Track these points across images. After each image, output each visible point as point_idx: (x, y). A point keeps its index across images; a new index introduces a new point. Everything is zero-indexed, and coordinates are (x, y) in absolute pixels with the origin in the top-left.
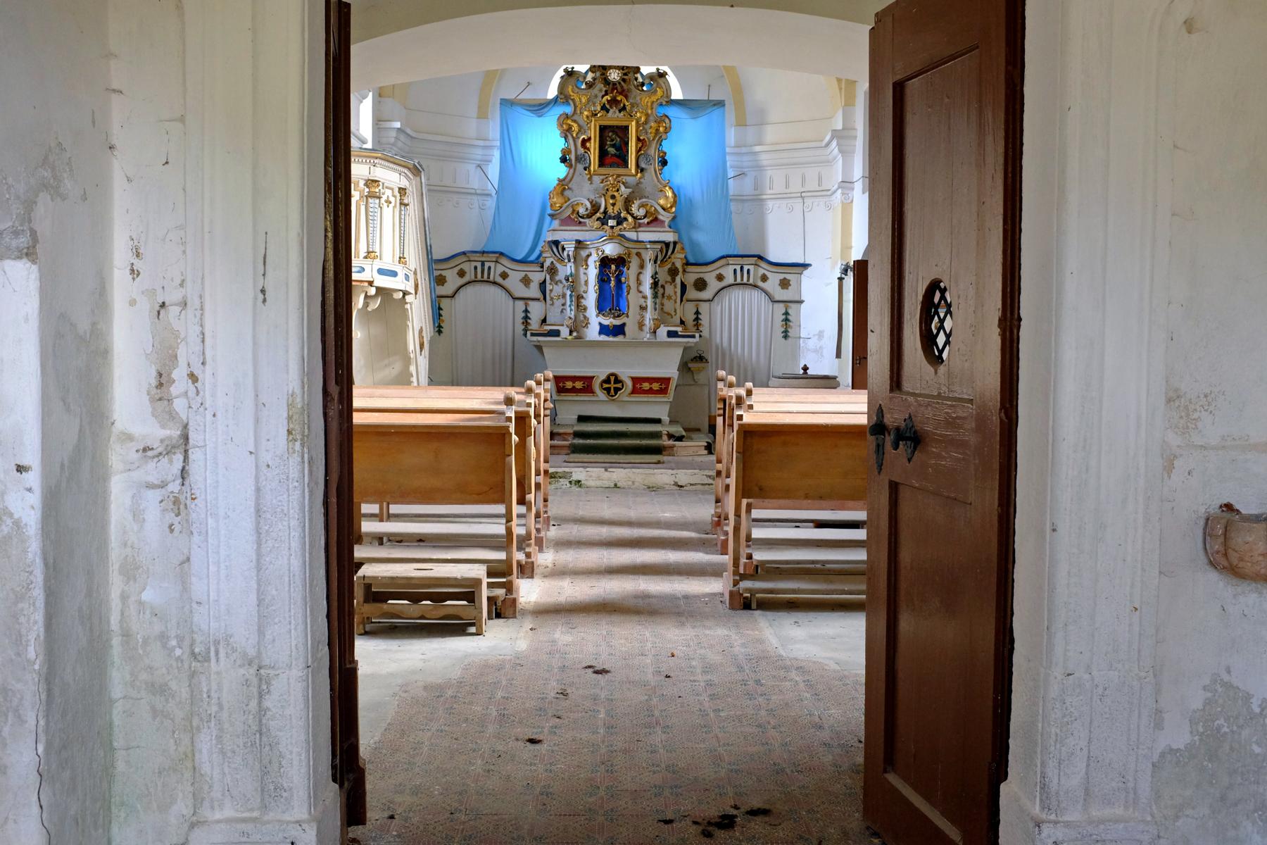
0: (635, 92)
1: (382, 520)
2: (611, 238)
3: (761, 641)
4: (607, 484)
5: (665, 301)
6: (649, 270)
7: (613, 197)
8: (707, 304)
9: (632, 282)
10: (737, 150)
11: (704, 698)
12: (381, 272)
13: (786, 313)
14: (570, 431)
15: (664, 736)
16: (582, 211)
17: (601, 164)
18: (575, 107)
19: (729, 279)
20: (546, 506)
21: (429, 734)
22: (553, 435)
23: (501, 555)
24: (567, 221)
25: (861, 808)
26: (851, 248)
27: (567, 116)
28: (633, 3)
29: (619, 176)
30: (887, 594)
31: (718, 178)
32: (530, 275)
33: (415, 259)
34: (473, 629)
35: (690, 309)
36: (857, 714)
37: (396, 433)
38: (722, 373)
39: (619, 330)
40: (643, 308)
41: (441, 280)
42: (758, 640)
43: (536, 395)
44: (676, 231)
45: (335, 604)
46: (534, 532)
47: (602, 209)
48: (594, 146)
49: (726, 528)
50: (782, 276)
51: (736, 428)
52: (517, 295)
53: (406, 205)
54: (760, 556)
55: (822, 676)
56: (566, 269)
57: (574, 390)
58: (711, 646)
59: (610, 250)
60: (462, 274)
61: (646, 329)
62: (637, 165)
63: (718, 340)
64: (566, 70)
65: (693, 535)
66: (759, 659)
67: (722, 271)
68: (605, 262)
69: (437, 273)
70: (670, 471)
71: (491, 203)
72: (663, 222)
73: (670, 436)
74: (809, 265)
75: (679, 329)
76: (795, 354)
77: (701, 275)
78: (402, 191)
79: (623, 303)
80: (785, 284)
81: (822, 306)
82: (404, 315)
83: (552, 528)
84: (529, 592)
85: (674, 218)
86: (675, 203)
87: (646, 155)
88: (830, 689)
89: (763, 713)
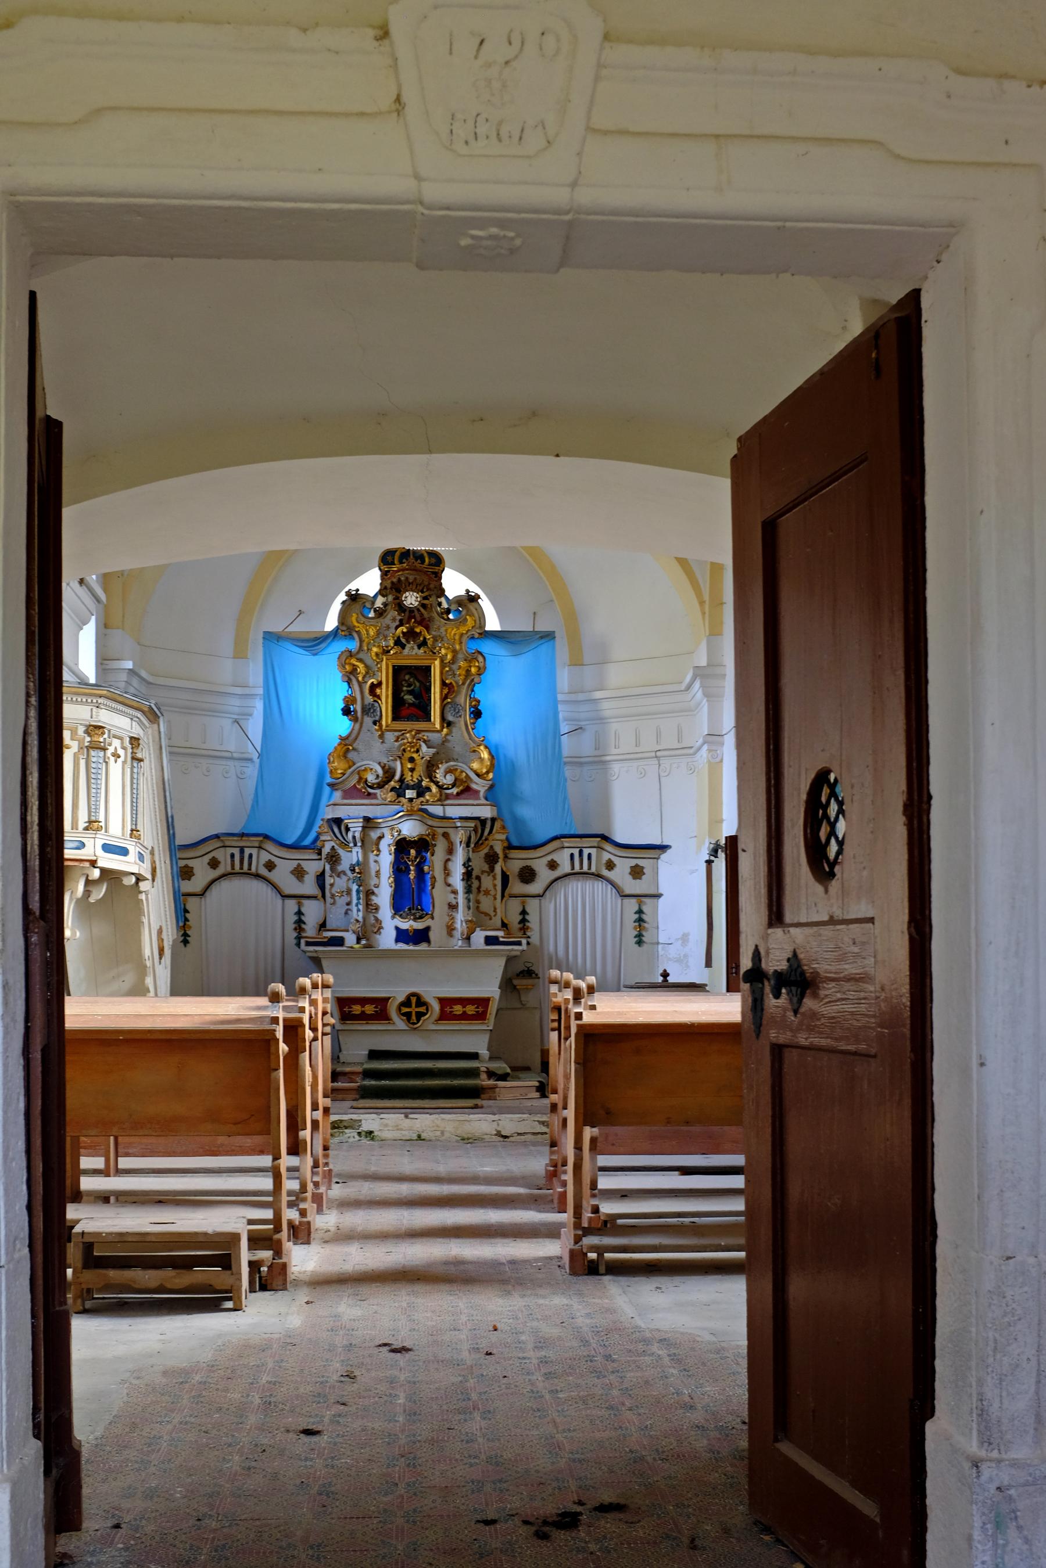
0: (439, 621)
1: (108, 1175)
2: (410, 814)
3: (613, 1311)
4: (407, 1135)
5: (482, 897)
6: (460, 856)
7: (412, 760)
8: (536, 901)
9: (438, 873)
10: (573, 697)
11: (538, 1377)
12: (107, 848)
13: (640, 912)
14: (359, 1069)
15: (484, 1424)
16: (371, 778)
17: (396, 717)
18: (361, 641)
19: (565, 867)
20: (326, 1156)
21: (170, 1427)
22: (335, 1076)
23: (268, 1214)
24: (352, 793)
25: (746, 1501)
26: (721, 821)
27: (350, 654)
28: (431, 452)
29: (419, 732)
30: (775, 1246)
31: (549, 736)
32: (303, 864)
33: (152, 834)
34: (229, 1304)
35: (515, 906)
36: (740, 1391)
37: (126, 1041)
38: (555, 973)
39: (421, 936)
40: (453, 907)
41: (186, 873)
42: (608, 1310)
43: (315, 1004)
44: (495, 804)
45: (39, 1189)
46: (310, 1186)
47: (397, 777)
48: (386, 693)
49: (564, 1177)
50: (633, 862)
51: (574, 1030)
52: (287, 891)
53: (141, 760)
54: (608, 1208)
55: (693, 1349)
56: (352, 856)
57: (363, 1017)
58: (546, 1318)
59: (410, 829)
60: (214, 864)
61: (457, 934)
62: (443, 718)
63: (552, 948)
64: (348, 593)
65: (522, 1190)
66: (608, 1331)
67: (555, 857)
68: (402, 846)
69: (182, 863)
70: (491, 1117)
71: (252, 771)
72: (477, 792)
73: (491, 1074)
74: (663, 848)
75: (500, 933)
76: (654, 957)
77: (529, 863)
78: (135, 741)
79: (426, 899)
80: (637, 872)
81: (685, 902)
82: (137, 908)
83: (335, 1186)
84: (303, 1260)
85: (492, 787)
86: (492, 768)
87: (455, 705)
88: (704, 1364)
89: (615, 1392)
